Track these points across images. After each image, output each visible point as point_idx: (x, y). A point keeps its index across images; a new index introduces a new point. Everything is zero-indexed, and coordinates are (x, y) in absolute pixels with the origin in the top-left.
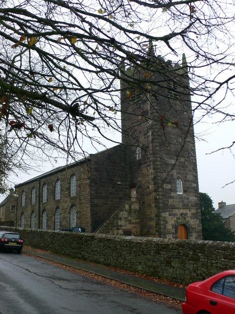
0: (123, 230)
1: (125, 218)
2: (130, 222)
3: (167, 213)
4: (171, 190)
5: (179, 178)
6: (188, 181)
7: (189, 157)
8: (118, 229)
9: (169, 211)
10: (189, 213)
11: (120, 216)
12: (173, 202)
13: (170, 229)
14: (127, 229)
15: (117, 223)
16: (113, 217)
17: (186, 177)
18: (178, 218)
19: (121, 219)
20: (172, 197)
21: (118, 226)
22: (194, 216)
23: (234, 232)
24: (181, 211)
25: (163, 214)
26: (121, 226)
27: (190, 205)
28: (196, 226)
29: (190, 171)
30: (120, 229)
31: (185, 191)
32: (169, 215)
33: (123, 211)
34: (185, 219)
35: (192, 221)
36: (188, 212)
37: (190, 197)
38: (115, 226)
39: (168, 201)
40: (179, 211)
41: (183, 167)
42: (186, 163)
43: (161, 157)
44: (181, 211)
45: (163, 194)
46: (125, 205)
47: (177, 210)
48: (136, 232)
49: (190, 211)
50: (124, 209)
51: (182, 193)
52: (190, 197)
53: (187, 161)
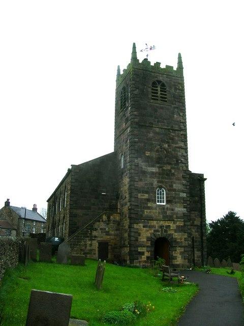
0: (98, 241)
1: (101, 229)
2: (108, 233)
3: (141, 225)
4: (148, 200)
5: (161, 187)
6: (175, 190)
7: (177, 163)
8: (91, 240)
9: (143, 223)
10: (173, 226)
11: (96, 226)
12: (150, 212)
13: (143, 242)
14: (102, 240)
15: (91, 234)
16: (86, 227)
17: (171, 186)
18: (158, 231)
19: (96, 230)
20: (149, 208)
21: (92, 237)
22: (179, 229)
23: (206, 179)
24: (162, 223)
25: (135, 226)
26: (95, 237)
27: (175, 216)
28: (183, 240)
29: (178, 179)
30: (94, 240)
31: (168, 202)
32: (144, 227)
33: (99, 221)
34: (166, 231)
35: (176, 234)
36: (171, 225)
37: (176, 208)
38: (88, 237)
39: (143, 212)
40: (157, 223)
41: (167, 175)
42: (173, 171)
43: (137, 164)
44: (162, 223)
45: (137, 204)
46: (102, 215)
47: (155, 222)
48: (115, 244)
49: (174, 223)
50: (101, 220)
51: (165, 204)
52: (176, 208)
53: (174, 168)
